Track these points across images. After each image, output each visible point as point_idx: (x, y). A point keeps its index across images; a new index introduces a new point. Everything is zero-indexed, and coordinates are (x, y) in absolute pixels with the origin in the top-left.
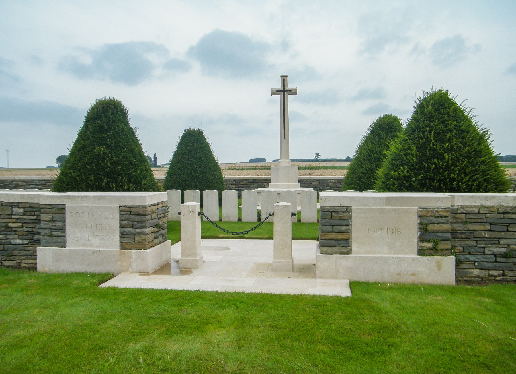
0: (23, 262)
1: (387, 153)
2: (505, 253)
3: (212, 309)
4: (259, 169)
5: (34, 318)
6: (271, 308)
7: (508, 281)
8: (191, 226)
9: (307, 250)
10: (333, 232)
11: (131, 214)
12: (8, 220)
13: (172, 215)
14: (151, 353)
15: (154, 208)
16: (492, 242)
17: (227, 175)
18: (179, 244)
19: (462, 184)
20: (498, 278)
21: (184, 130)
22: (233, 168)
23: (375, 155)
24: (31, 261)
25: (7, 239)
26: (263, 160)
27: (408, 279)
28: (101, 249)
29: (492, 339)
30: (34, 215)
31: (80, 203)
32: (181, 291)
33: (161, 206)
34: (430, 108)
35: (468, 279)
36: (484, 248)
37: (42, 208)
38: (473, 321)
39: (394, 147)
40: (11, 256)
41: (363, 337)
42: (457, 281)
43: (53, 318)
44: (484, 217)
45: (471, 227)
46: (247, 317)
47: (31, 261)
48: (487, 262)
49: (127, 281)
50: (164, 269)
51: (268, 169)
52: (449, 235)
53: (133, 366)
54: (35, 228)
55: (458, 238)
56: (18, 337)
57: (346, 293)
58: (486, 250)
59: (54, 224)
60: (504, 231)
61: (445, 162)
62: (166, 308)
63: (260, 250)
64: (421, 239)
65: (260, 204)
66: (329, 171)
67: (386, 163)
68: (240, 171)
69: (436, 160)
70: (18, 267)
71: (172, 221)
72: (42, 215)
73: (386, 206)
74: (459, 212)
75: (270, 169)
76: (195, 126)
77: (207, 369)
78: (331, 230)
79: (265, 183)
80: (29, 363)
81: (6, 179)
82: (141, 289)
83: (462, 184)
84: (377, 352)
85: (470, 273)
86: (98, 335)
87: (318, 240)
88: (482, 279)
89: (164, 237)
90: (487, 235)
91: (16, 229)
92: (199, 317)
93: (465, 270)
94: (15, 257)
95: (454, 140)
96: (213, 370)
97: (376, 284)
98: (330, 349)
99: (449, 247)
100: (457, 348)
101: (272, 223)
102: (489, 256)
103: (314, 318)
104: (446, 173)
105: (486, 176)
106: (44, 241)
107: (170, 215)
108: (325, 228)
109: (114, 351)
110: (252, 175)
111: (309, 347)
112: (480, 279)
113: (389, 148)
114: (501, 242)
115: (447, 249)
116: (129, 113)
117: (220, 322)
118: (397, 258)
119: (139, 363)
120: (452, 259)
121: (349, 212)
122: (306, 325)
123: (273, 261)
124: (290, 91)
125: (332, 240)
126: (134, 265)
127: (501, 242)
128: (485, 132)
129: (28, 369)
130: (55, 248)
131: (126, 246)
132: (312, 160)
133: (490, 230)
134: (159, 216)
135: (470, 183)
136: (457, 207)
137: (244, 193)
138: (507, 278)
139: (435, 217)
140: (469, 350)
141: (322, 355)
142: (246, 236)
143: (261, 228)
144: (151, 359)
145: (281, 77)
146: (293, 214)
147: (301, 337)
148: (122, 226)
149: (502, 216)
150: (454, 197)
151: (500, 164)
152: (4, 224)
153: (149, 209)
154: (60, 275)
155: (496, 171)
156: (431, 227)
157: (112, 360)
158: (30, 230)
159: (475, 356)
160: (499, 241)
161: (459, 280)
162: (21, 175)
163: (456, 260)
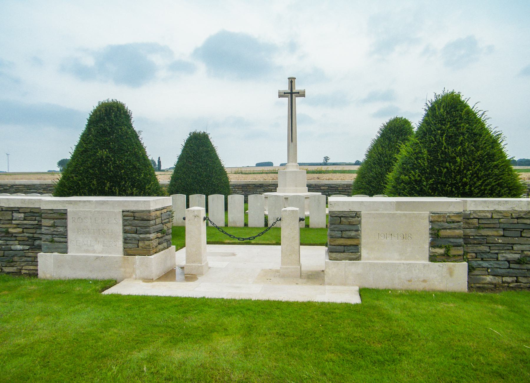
0: (24, 268)
1: (398, 156)
2: (518, 259)
3: (218, 317)
4: (266, 173)
6: (278, 316)
7: (521, 288)
8: (196, 232)
9: (315, 256)
10: (342, 238)
11: (134, 219)
12: (8, 226)
13: (177, 220)
14: (156, 361)
15: (158, 213)
16: (506, 248)
17: (233, 179)
18: (184, 249)
19: (475, 189)
20: (511, 285)
22: (239, 172)
24: (32, 268)
25: (7, 245)
26: (270, 164)
27: (419, 286)
28: (104, 255)
29: (506, 347)
30: (35, 220)
32: (185, 298)
33: (165, 210)
34: (442, 110)
35: (481, 285)
36: (497, 254)
37: (43, 213)
38: (486, 329)
39: (404, 150)
40: (12, 262)
42: (470, 288)
43: (55, 326)
44: (497, 222)
47: (32, 268)
48: (500, 268)
49: (129, 288)
50: (169, 275)
51: (275, 173)
52: (461, 241)
53: (136, 375)
55: (470, 244)
56: (19, 345)
57: (356, 300)
58: (499, 256)
59: (55, 229)
60: (517, 237)
61: (457, 166)
62: (171, 316)
63: (266, 256)
64: (433, 245)
65: (267, 209)
66: (338, 175)
67: (396, 167)
68: (246, 175)
69: (447, 164)
70: (19, 273)
71: (176, 227)
73: (397, 211)
74: (472, 217)
75: (277, 173)
76: (200, 130)
77: (213, 378)
78: (340, 235)
79: (272, 187)
80: (29, 371)
81: (6, 183)
82: (145, 296)
83: (475, 189)
84: (387, 361)
85: (483, 279)
86: (100, 343)
87: (326, 245)
88: (495, 286)
89: (169, 243)
90: (500, 241)
92: (204, 324)
93: (478, 277)
94: (15, 263)
95: (467, 144)
96: (219, 379)
97: (386, 291)
99: (461, 253)
100: (469, 356)
101: (279, 229)
102: (503, 262)
103: (322, 326)
105: (499, 180)
106: (45, 246)
107: (174, 221)
108: (333, 233)
109: (118, 359)
110: (259, 179)
115: (459, 255)
116: (133, 116)
118: (408, 264)
119: (143, 371)
120: (464, 265)
121: (358, 217)
122: (315, 333)
123: (281, 268)
124: (298, 93)
125: (341, 245)
126: (138, 272)
127: (515, 247)
128: (498, 135)
129: (29, 378)
130: (56, 254)
131: (130, 252)
132: (320, 164)
133: (503, 236)
134: (163, 221)
135: (483, 188)
136: (469, 212)
137: (251, 197)
138: (520, 285)
139: (447, 222)
140: (481, 358)
141: (331, 363)
142: (253, 242)
143: (268, 233)
144: (155, 367)
145: (289, 79)
146: (301, 220)
147: (309, 345)
148: (125, 232)
149: (516, 221)
150: (466, 202)
151: (514, 168)
152: (4, 230)
153: (153, 214)
154: (62, 282)
155: (509, 175)
156: (443, 233)
157: (115, 369)
158: (31, 235)
159: (488, 364)
160: (512, 247)
162: (22, 179)
163: (469, 266)
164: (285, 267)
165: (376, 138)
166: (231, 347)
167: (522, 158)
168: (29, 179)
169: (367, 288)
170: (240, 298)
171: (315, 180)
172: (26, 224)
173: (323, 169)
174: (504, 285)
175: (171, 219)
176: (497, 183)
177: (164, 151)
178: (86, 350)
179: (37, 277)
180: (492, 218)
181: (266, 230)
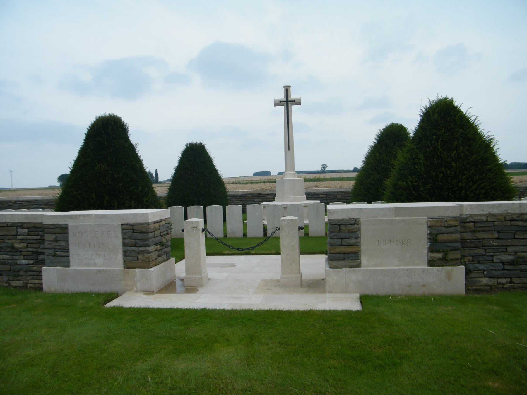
0: (29, 282)
1: (395, 163)
2: (512, 260)
3: (219, 327)
4: (264, 182)
5: (43, 337)
6: (279, 325)
7: (515, 288)
8: (195, 243)
9: (315, 265)
10: (342, 245)
11: (133, 232)
12: (13, 241)
13: (175, 232)
14: (160, 372)
15: (157, 225)
16: (500, 250)
17: (231, 189)
18: (183, 261)
19: (470, 193)
20: (505, 286)
21: (185, 144)
22: (237, 182)
23: (383, 165)
24: (37, 281)
25: (13, 259)
26: (268, 173)
27: (418, 291)
28: (104, 269)
29: (501, 345)
30: (38, 235)
31: (85, 219)
32: (187, 310)
33: (163, 223)
34: (436, 116)
35: (478, 288)
36: (492, 256)
37: (45, 228)
38: (483, 329)
39: (401, 156)
40: (18, 276)
41: (374, 351)
42: (467, 290)
43: (61, 338)
44: (492, 225)
45: (480, 235)
46: (256, 335)
47: (37, 281)
48: (495, 270)
49: (133, 300)
50: (169, 287)
51: (273, 182)
52: (458, 245)
53: (141, 385)
54: (39, 248)
55: (467, 247)
56: (29, 356)
57: (356, 306)
58: (495, 258)
59: (57, 244)
60: (511, 239)
61: (453, 171)
62: (173, 327)
63: (266, 266)
64: (431, 250)
65: (265, 218)
66: (336, 182)
67: (394, 173)
68: (244, 185)
69: (443, 169)
70: (25, 287)
71: (175, 239)
72: (46, 235)
73: (396, 217)
74: (468, 221)
75: (275, 182)
76: (196, 140)
77: (216, 387)
78: (340, 243)
79: (271, 196)
80: (40, 381)
81: (10, 199)
82: (146, 308)
83: (470, 193)
84: (388, 365)
85: (480, 281)
86: (105, 355)
87: (326, 254)
88: (491, 287)
89: (168, 255)
90: (495, 244)
91: (22, 250)
92: (206, 335)
93: (475, 279)
94: (21, 277)
95: (461, 148)
96: (223, 388)
97: (386, 297)
98: (341, 363)
99: (459, 256)
100: (466, 356)
101: (278, 238)
102: (498, 264)
103: (324, 333)
104: (455, 181)
105: (493, 183)
106: (49, 261)
107: (173, 233)
108: (333, 241)
109: (123, 370)
110: (257, 188)
111: (320, 363)
112: (489, 288)
113: (396, 157)
114: (509, 249)
115: (457, 259)
116: (129, 129)
117: (228, 340)
118: (408, 270)
119: (148, 381)
120: (462, 268)
121: (357, 224)
122: (317, 341)
123: (281, 277)
124: (294, 101)
125: (341, 253)
126: (138, 284)
127: (509, 249)
128: (490, 139)
129: (40, 387)
130: (59, 268)
131: (130, 265)
132: (318, 172)
133: (498, 238)
134: (162, 234)
135: (478, 191)
136: (465, 216)
137: (249, 207)
138: (514, 285)
139: (444, 227)
140: (478, 358)
141: (333, 370)
142: (252, 252)
143: (265, 244)
144: (159, 378)
145: (284, 87)
146: (300, 228)
147: (311, 353)
148: (125, 245)
149: (509, 223)
150: (462, 206)
151: (507, 171)
152: (10, 245)
153: (152, 227)
154: (64, 295)
155: (502, 178)
156: (441, 237)
157: (120, 379)
158: (35, 250)
159: (484, 363)
160: (506, 249)
161: (469, 290)
162: (25, 195)
163: (466, 269)
164: (285, 276)
165: (373, 145)
166: (233, 357)
167: (514, 162)
168: (32, 195)
169: (368, 295)
170: (241, 309)
171: (313, 187)
172: (30, 239)
173: (321, 177)
174: (499, 286)
175: (169, 231)
176: (491, 186)
177: (160, 161)
178: (92, 361)
179: (42, 291)
180: (487, 221)
181: (266, 240)
